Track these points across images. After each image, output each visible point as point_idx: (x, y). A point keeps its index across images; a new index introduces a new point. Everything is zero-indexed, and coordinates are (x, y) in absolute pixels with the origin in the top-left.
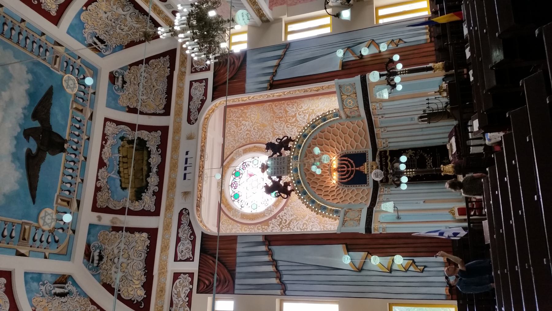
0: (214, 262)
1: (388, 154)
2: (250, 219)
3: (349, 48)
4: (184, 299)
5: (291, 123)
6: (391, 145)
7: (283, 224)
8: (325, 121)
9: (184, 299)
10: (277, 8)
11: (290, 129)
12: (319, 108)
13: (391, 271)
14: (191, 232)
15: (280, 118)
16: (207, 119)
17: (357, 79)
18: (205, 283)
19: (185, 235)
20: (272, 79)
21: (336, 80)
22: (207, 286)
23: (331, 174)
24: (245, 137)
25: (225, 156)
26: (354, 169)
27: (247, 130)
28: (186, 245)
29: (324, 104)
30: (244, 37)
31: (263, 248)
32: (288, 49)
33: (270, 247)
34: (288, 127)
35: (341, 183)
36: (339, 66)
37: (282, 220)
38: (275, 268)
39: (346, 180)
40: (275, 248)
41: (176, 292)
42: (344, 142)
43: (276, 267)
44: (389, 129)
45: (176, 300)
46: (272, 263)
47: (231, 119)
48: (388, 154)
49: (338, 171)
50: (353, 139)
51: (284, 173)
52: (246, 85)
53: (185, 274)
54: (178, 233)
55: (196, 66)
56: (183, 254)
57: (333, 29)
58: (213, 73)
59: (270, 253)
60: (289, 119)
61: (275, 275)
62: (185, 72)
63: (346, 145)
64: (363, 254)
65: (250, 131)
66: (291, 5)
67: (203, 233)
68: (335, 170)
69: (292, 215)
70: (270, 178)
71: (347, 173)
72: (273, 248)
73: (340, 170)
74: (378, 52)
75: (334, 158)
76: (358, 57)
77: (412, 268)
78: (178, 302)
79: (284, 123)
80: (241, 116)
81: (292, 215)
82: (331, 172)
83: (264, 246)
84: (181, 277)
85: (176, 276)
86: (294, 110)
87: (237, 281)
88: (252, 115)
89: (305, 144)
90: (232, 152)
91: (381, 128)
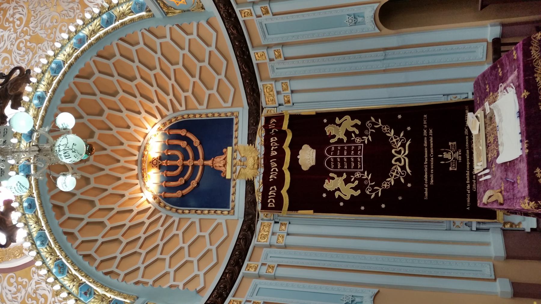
1: (285, 126)
6: (296, 97)
23: (142, 176)
26: (200, 162)
27: (6, 51)
39: (179, 194)
44: (289, 52)
48: (285, 126)
49: (160, 167)
50: (197, 79)
65: (10, 52)
68: (154, 163)
71: (182, 174)
73: (164, 163)
82: (142, 169)
88: (17, 16)
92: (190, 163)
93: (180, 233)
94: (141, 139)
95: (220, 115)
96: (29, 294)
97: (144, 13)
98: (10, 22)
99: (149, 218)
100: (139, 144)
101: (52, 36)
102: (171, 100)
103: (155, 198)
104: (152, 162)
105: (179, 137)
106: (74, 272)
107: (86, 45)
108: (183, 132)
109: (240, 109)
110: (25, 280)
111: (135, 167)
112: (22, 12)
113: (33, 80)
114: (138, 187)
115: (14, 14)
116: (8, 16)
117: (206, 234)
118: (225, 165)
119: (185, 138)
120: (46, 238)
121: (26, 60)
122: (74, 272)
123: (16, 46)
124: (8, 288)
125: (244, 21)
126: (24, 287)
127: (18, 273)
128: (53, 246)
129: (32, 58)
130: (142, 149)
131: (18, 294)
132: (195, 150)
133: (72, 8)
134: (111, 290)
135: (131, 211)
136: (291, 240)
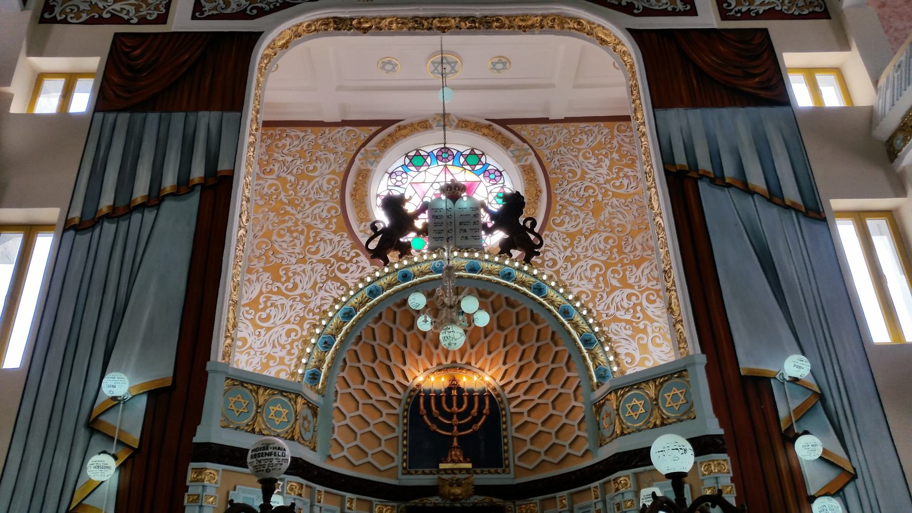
2: (355, 190)
3: (821, 397)
5: (604, 275)
7: (336, 266)
11: (588, 273)
12: (651, 346)
18: (135, 48)
21: (703, 359)
22: (616, 391)
23: (441, 369)
24: (567, 168)
25: (516, 128)
27: (584, 173)
29: (645, 336)
31: (198, 172)
32: (806, 215)
33: (198, 188)
34: (592, 268)
35: (418, 396)
36: (752, 366)
37: (347, 262)
38: (139, 201)
40: (192, 203)
42: (533, 404)
43: (142, 207)
46: (154, 194)
47: (616, 132)
49: (449, 389)
51: (436, 239)
52: (682, 110)
57: (883, 348)
58: (716, 26)
61: (121, 204)
63: (524, 409)
64: (134, 434)
65: (583, 178)
67: (259, 34)
70: (424, 207)
72: (194, 200)
73: (454, 392)
74: (812, 491)
75: (487, 378)
76: (791, 428)
79: (604, 258)
80: (622, 157)
82: (447, 368)
83: (202, 175)
86: (644, 282)
88: (626, 182)
90: (524, 141)
93: (384, 418)
94: (478, 366)
95: (507, 451)
96: (319, 233)
97: (595, 380)
98: (617, 173)
99: (399, 383)
100: (473, 364)
101: (602, 228)
102: (519, 397)
103: (418, 385)
104: (454, 380)
106: (345, 329)
107: (563, 320)
108: (486, 410)
109: (512, 475)
110: (334, 227)
111: (449, 362)
112: (630, 186)
113: (526, 268)
114: (429, 366)
115: (627, 177)
116: (626, 170)
118: (453, 461)
119: (480, 412)
120: (375, 296)
121: (573, 199)
123: (590, 184)
124: (326, 208)
125: (590, 489)
126: (327, 227)
127: (341, 217)
128: (368, 304)
129: (576, 207)
130: (466, 367)
131: (319, 221)
133: (635, 249)
134: (329, 368)
135: (405, 364)
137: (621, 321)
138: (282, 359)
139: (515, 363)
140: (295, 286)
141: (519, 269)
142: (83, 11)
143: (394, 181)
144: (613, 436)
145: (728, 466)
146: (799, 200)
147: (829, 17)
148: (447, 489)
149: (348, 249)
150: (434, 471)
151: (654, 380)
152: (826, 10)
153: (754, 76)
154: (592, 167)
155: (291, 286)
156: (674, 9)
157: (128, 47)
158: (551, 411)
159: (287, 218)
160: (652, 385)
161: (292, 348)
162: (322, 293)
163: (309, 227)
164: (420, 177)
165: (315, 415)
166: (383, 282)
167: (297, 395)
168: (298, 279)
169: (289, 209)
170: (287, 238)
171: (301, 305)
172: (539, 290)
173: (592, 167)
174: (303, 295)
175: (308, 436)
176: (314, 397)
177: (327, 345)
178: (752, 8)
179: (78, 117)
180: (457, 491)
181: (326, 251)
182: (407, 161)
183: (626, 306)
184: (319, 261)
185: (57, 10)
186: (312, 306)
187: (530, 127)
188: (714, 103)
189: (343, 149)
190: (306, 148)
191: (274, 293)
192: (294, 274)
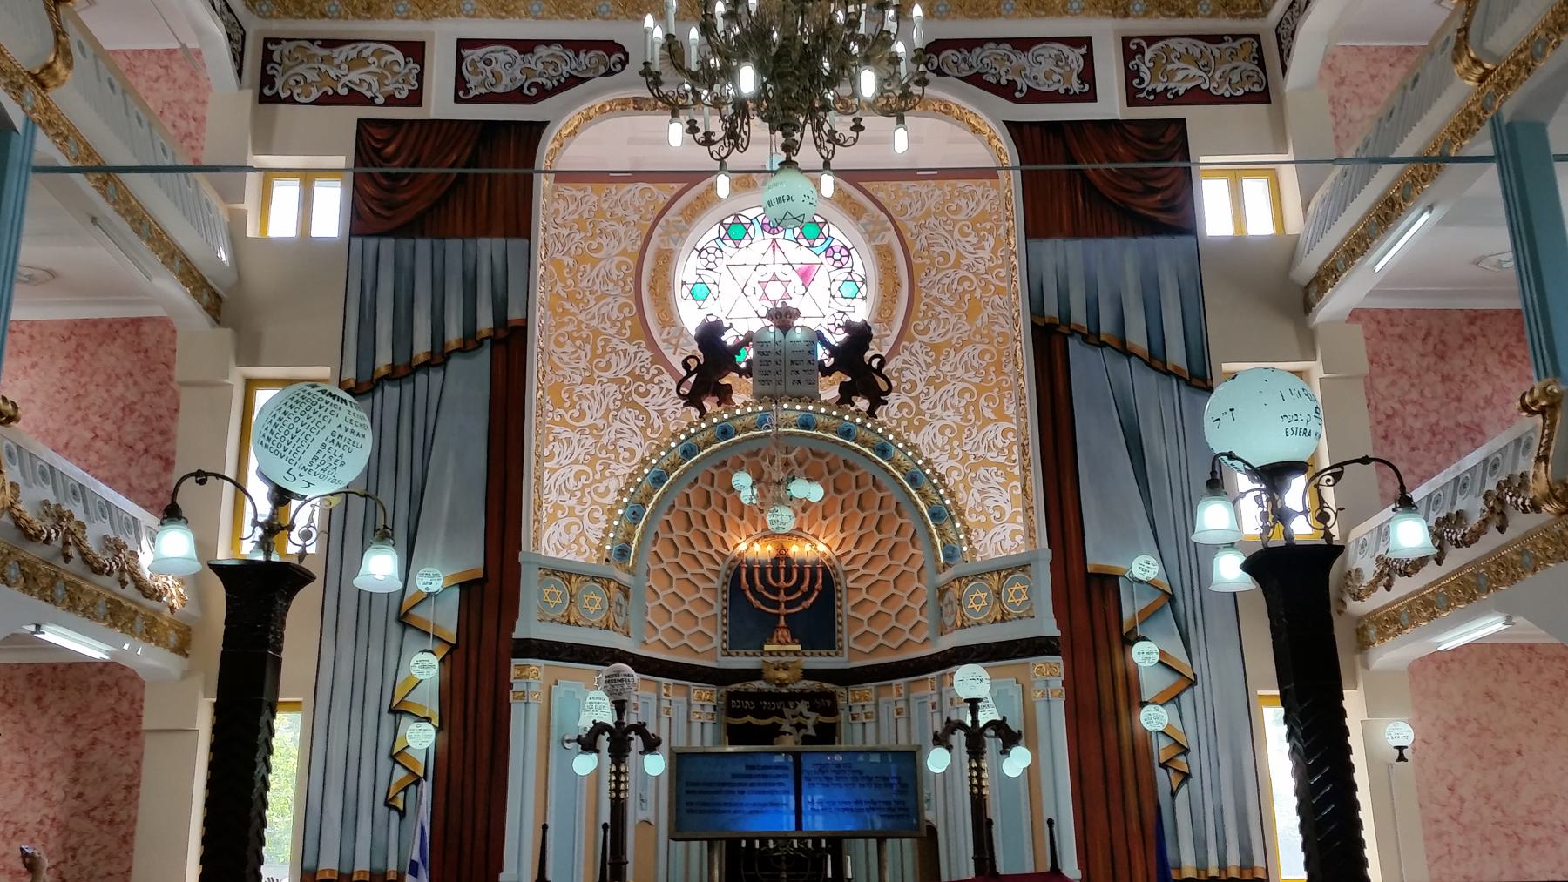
0: (452, 166)
2: (653, 280)
3: (1171, 598)
4: (344, 80)
5: (976, 404)
6: (858, 728)
7: (633, 387)
8: (934, 516)
9: (344, 80)
10: (1355, 345)
11: (956, 401)
13: (396, 711)
14: (549, 85)
15: (998, 365)
16: (946, 110)
17: (1048, 627)
18: (387, 142)
19: (540, 66)
20: (1073, 332)
22: (377, 151)
24: (937, 249)
25: (871, 186)
27: (960, 256)
28: (508, 71)
29: (1000, 518)
30: (1260, 224)
31: (485, 322)
32: (1188, 383)
33: (488, 342)
34: (961, 394)
35: (739, 568)
37: (647, 382)
38: (422, 359)
40: (482, 360)
41: (366, 53)
42: (873, 580)
43: (427, 366)
44: (902, 724)
45: (343, 57)
46: (438, 350)
49: (776, 560)
51: (762, 382)
52: (1060, 241)
53: (420, 77)
54: (548, 43)
55: (1149, 53)
56: (481, 65)
59: (471, 345)
60: (990, 399)
62: (1126, 15)
63: (863, 585)
64: (450, 630)
65: (957, 265)
66: (1370, 389)
67: (544, 124)
68: (782, 550)
69: (661, 412)
70: (749, 339)
71: (768, 587)
72: (484, 356)
73: (782, 564)
75: (822, 548)
76: (1133, 630)
77: (400, 773)
78: (336, 62)
79: (977, 380)
81: (661, 412)
83: (491, 325)
84: (411, 65)
85: (415, 51)
87: (387, 245)
89: (857, 450)
91: (908, 701)
92: (782, 597)
93: (701, 594)
104: (783, 548)
105: (814, 579)
106: (656, 496)
108: (819, 585)
117: (700, 627)
122: (656, 496)
124: (617, 305)
126: (619, 333)
132: (797, 602)
134: (639, 542)
135: (724, 530)
136: (696, 728)
137: (992, 464)
138: (572, 509)
139: (854, 531)
140: (582, 415)
141: (862, 425)
142: (312, 84)
143: (705, 262)
144: (955, 627)
145: (1061, 670)
146: (1184, 366)
147: (1269, 102)
148: (772, 673)
149: (647, 363)
150: (758, 652)
151: (999, 572)
152: (1266, 92)
153: (1156, 191)
154: (970, 249)
155: (577, 414)
156: (1067, 90)
157: (377, 141)
158: (893, 590)
159: (566, 319)
160: (996, 576)
161: (583, 495)
162: (617, 425)
163: (597, 332)
164: (741, 256)
165: (626, 597)
166: (700, 438)
167: (609, 580)
168: (585, 404)
169: (568, 306)
170: (569, 348)
171: (591, 440)
172: (883, 451)
173: (970, 249)
174: (593, 427)
175: (620, 622)
176: (625, 578)
177: (636, 516)
178: (1171, 85)
179: (325, 243)
180: (783, 675)
181: (620, 367)
182: (723, 232)
183: (1000, 445)
184: (610, 380)
185: (279, 82)
186: (605, 440)
187: (890, 186)
188: (1101, 232)
189: (636, 217)
190: (586, 215)
191: (557, 424)
192: (580, 397)
